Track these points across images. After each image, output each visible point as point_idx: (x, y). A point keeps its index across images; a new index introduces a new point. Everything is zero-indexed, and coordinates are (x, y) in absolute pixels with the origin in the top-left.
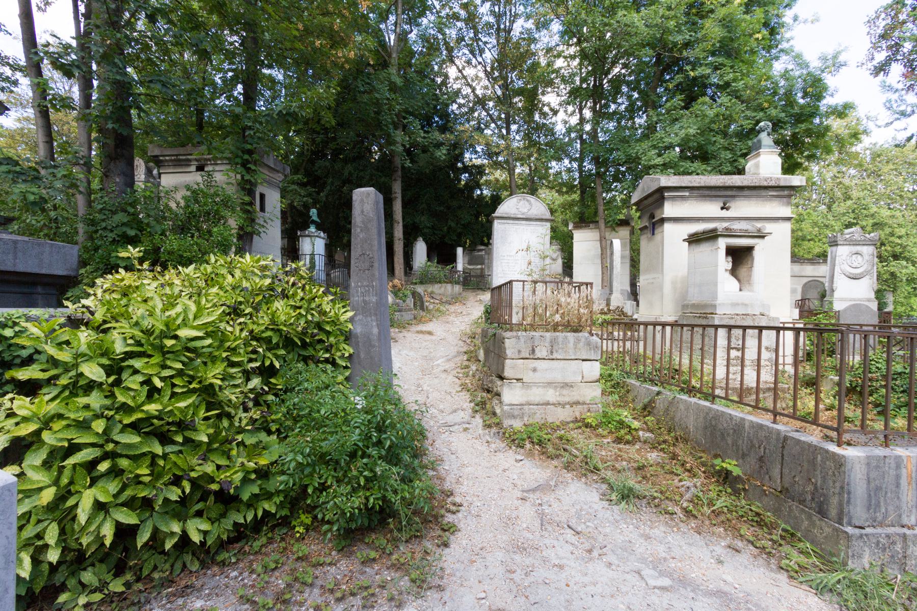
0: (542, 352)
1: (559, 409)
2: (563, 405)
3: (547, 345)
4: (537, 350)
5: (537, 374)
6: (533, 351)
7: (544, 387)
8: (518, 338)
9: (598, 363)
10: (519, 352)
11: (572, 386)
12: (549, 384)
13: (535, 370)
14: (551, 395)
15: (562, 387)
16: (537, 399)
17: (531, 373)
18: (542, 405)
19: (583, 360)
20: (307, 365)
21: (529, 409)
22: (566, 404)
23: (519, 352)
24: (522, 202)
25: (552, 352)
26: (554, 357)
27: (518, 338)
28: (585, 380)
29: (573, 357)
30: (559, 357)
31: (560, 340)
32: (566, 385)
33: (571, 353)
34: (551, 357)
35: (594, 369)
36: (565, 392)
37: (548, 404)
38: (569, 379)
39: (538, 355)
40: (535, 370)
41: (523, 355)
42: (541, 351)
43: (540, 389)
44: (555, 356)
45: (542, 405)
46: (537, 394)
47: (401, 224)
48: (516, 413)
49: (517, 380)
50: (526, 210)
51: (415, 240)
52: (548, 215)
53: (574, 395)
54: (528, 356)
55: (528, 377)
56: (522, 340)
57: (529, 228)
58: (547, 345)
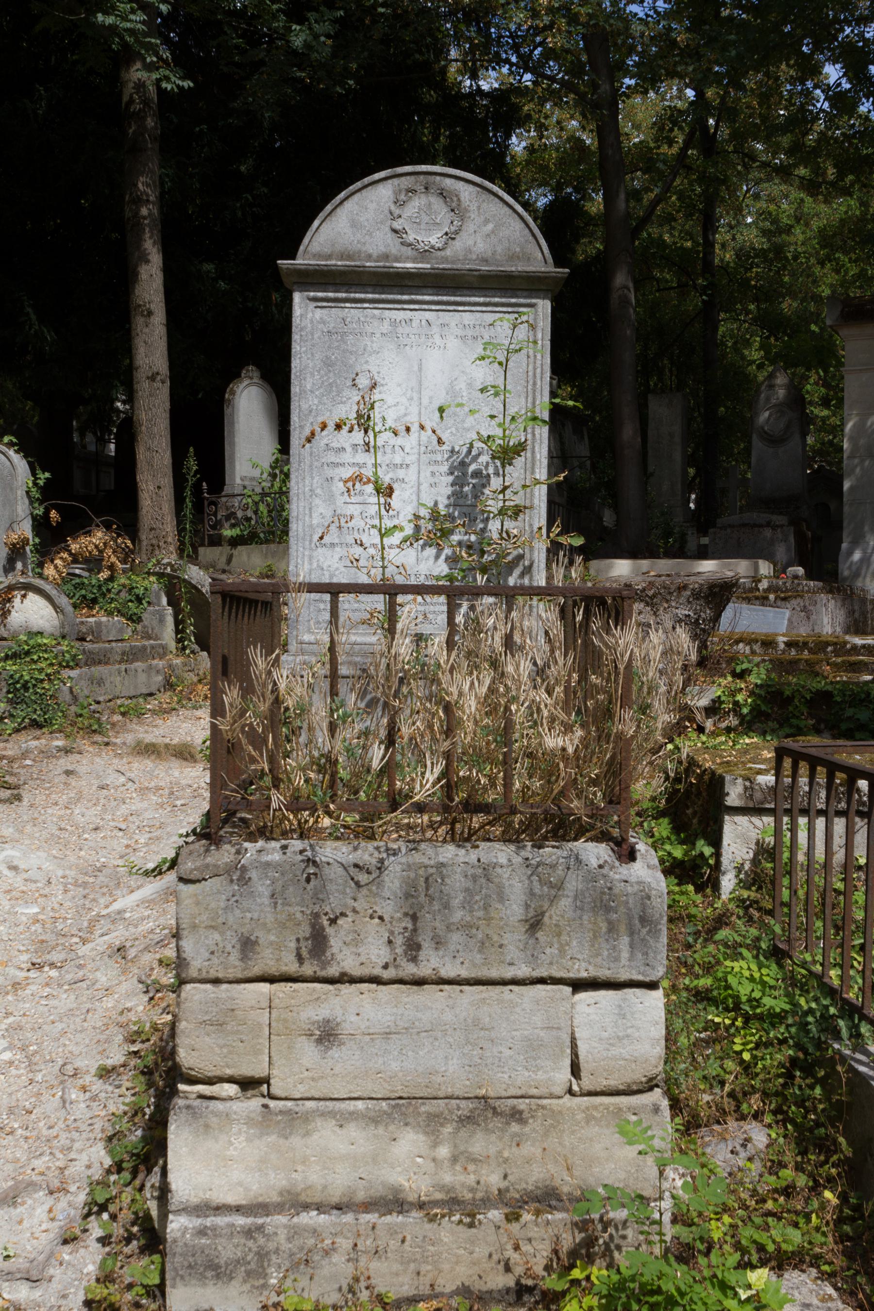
0: (362, 946)
1: (448, 1233)
2: (463, 1208)
3: (387, 909)
4: (336, 940)
5: (344, 1058)
6: (318, 942)
7: (375, 1120)
8: (239, 875)
9: (656, 999)
10: (248, 945)
11: (516, 1116)
12: (403, 1107)
13: (327, 1035)
14: (410, 1161)
15: (467, 1120)
16: (339, 1181)
17: (308, 1052)
18: (368, 1206)
19: (579, 985)
20: (696, 595)
21: (294, 1232)
22: (486, 1203)
23: (248, 945)
24: (417, 203)
25: (413, 949)
26: (424, 970)
27: (239, 875)
28: (587, 1083)
29: (523, 971)
30: (449, 971)
31: (456, 882)
32: (487, 1110)
33: (512, 952)
34: (410, 970)
35: (632, 1028)
36: (480, 1143)
37: (394, 1203)
38: (508, 1077)
39: (345, 959)
40: (327, 1035)
41: (266, 961)
42: (357, 940)
43: (353, 1131)
44: (431, 962)
45: (368, 1206)
46: (338, 1156)
47: (159, 318)
48: (227, 1251)
49: (248, 1084)
50: (434, 239)
51: (235, 375)
52: (538, 258)
53: (532, 1161)
54: (291, 967)
55: (297, 1070)
56: (262, 887)
57: (452, 319)
58: (387, 909)
